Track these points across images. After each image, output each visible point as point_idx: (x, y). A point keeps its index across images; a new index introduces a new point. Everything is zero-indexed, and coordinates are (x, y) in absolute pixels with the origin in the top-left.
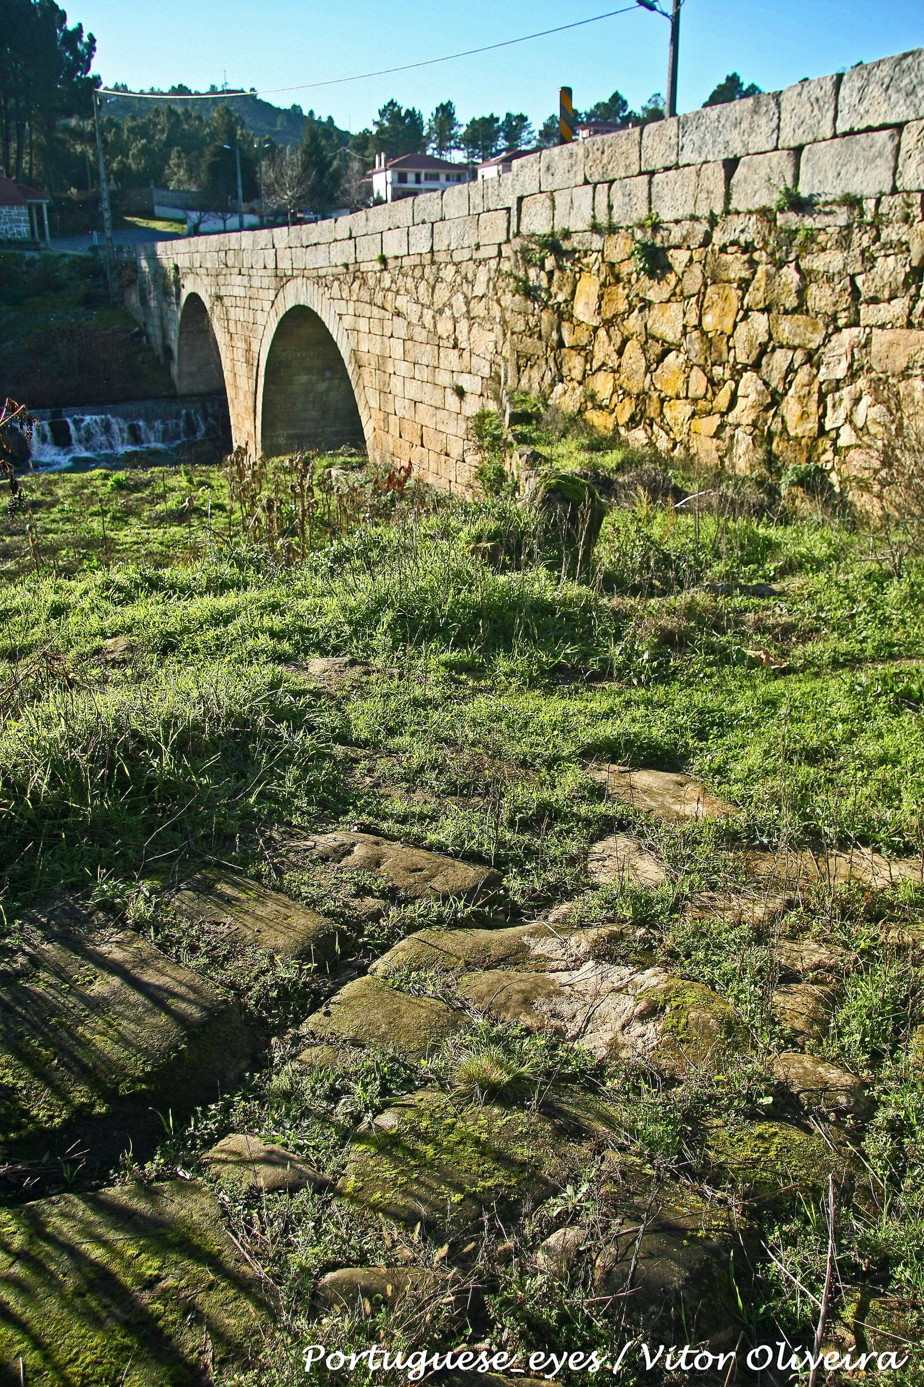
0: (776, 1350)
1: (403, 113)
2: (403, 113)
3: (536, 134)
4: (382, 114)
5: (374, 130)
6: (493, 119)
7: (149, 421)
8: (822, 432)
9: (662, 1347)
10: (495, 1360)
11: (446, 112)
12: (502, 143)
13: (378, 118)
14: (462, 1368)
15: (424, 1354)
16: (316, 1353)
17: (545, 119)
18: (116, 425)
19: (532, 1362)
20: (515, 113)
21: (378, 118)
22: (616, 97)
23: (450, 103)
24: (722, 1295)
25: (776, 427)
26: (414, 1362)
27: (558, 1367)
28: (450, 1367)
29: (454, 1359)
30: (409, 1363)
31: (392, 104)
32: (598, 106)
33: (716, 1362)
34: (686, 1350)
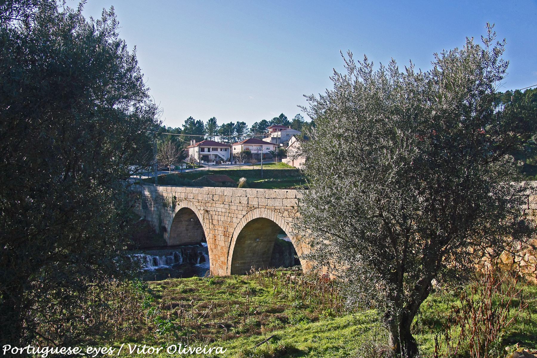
1: (196, 121)
2: (196, 121)
3: (249, 129)
4: (186, 122)
5: (183, 129)
6: (231, 124)
7: (161, 256)
8: (514, 262)
11: (213, 122)
12: (235, 134)
13: (184, 124)
15: (47, 348)
16: (8, 347)
17: (253, 124)
18: (149, 258)
20: (241, 121)
21: (184, 124)
22: (282, 115)
25: (499, 261)
26: (44, 351)
31: (191, 118)
32: (275, 119)
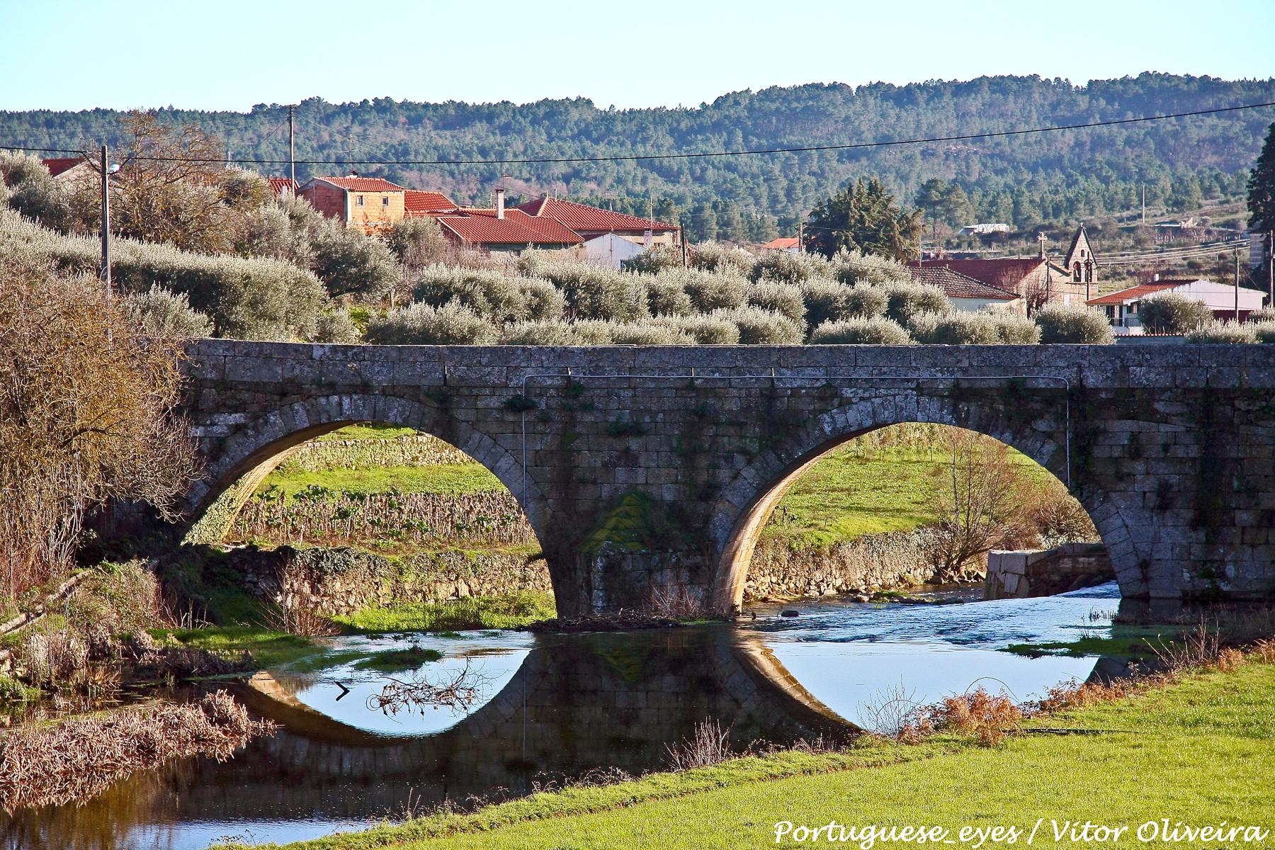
0: (1161, 825)
9: (1068, 823)
10: (931, 833)
14: (905, 840)
24: (194, 847)
27: (983, 839)
28: (895, 839)
29: (897, 834)
30: (861, 836)
33: (811, 835)
34: (1087, 826)
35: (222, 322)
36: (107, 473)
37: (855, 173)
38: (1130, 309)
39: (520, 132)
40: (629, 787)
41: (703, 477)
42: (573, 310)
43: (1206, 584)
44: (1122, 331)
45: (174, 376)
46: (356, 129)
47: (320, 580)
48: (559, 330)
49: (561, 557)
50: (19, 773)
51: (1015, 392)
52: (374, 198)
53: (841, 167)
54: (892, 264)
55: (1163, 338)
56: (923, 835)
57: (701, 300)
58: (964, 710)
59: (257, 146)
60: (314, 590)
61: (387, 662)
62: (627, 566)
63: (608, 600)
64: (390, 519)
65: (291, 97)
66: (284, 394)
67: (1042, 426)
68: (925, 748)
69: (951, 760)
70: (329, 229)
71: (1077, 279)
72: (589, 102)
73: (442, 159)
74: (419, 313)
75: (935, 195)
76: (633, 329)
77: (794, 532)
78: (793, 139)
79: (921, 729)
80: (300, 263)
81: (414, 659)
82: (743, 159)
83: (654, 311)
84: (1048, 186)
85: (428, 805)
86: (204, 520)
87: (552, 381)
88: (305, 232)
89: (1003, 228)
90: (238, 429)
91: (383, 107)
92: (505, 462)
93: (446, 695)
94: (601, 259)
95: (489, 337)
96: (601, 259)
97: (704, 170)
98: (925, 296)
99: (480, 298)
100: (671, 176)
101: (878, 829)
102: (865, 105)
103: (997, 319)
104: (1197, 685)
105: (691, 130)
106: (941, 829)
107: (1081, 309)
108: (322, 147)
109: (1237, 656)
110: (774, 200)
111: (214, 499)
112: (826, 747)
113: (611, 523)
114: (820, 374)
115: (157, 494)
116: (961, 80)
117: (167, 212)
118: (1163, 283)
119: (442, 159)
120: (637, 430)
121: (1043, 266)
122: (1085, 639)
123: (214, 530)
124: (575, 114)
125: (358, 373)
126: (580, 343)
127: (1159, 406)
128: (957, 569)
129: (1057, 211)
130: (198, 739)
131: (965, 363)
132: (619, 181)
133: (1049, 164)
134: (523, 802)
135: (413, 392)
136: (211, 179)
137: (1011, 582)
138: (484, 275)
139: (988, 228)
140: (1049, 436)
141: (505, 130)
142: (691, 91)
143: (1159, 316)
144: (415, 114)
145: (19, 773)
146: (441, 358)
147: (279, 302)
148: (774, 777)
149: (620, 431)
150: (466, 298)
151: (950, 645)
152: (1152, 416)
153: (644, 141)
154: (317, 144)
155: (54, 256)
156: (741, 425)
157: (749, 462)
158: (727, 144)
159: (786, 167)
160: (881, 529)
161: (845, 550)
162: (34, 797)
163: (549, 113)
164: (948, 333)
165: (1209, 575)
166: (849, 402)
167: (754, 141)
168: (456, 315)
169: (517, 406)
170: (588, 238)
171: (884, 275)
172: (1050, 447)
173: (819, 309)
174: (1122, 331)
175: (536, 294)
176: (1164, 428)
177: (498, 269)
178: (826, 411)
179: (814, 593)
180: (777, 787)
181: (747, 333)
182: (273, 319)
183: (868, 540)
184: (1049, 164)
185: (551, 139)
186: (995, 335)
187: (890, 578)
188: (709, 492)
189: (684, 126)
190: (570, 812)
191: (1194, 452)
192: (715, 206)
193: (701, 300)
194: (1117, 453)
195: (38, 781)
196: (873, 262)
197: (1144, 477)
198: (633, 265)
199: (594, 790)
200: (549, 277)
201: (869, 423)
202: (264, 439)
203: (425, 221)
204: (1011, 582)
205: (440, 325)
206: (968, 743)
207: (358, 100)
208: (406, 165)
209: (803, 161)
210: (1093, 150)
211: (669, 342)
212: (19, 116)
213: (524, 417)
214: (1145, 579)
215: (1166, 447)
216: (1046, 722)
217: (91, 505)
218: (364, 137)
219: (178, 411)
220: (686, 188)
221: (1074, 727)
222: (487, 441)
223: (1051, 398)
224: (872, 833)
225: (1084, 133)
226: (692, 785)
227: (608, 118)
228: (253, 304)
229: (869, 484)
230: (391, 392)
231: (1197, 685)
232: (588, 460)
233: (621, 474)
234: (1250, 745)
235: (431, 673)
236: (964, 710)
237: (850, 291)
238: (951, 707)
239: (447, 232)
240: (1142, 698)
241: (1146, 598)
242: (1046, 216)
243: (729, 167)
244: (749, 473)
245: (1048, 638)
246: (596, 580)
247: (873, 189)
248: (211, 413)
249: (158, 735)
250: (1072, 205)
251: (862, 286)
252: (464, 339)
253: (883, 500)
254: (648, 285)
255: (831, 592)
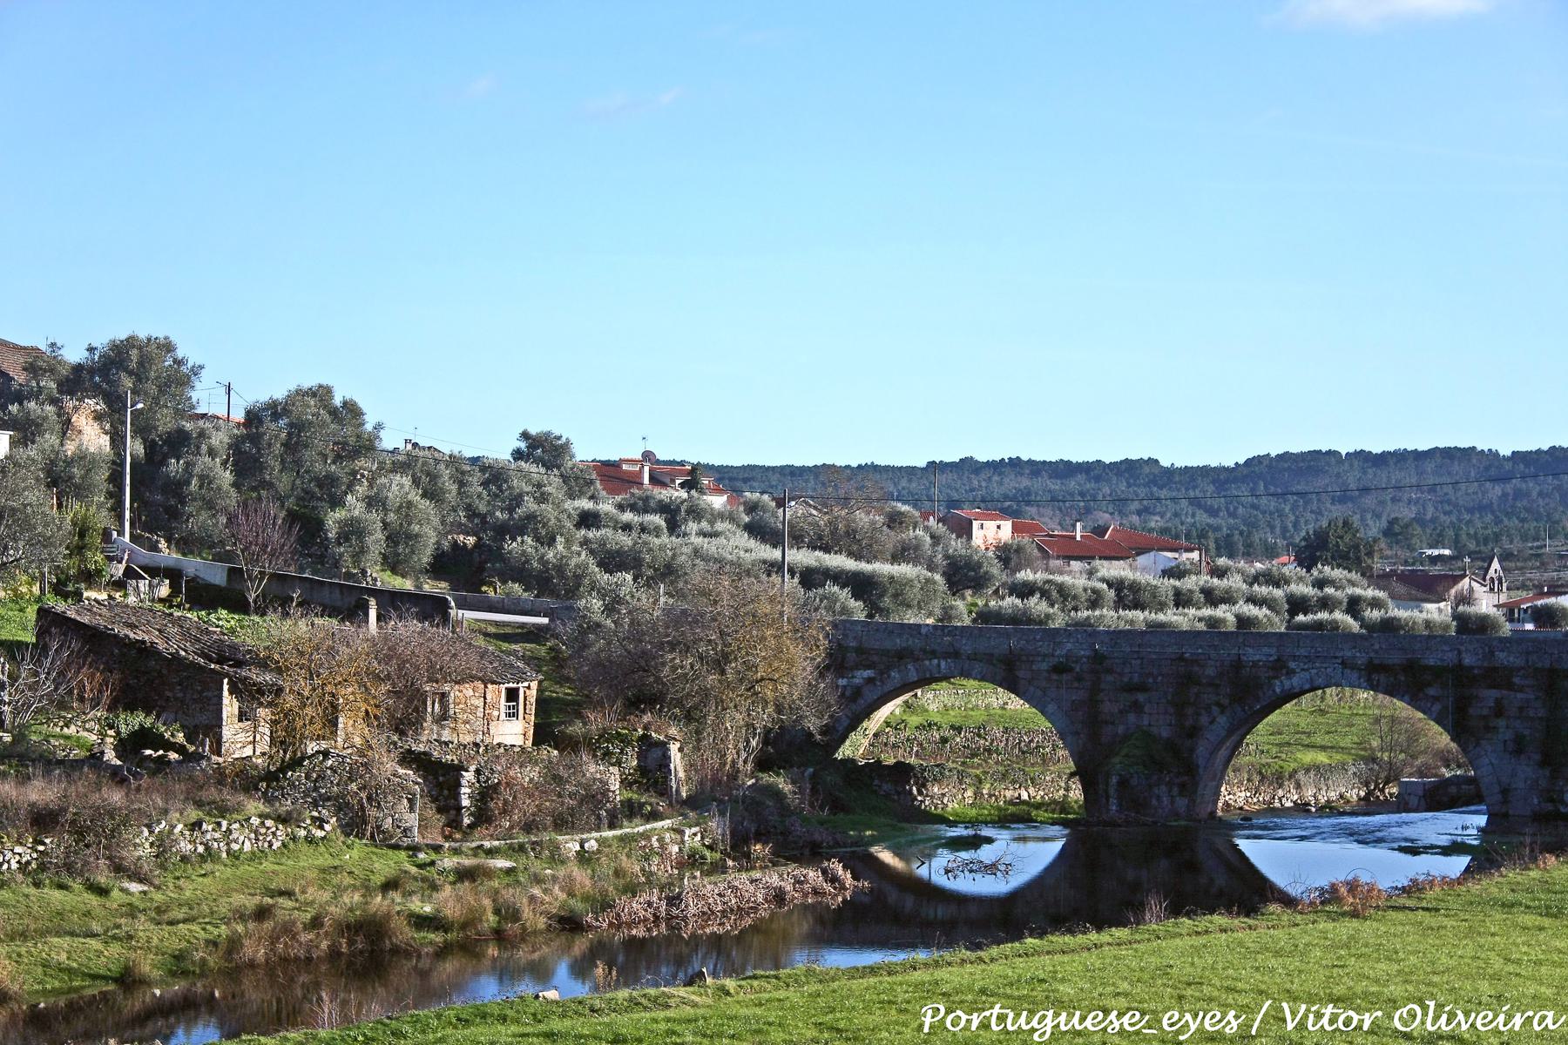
0: (1425, 1009)
10: (1126, 1020)
19: (1165, 1022)
23: (201, 367)
29: (1083, 1019)
30: (1034, 1023)
35: (873, 608)
36: (779, 709)
37: (1337, 512)
38: (1526, 611)
39: (1109, 481)
40: (1093, 936)
41: (1188, 723)
42: (1120, 603)
43: (1550, 807)
44: (1518, 627)
45: (824, 643)
46: (996, 478)
47: (924, 786)
48: (1109, 617)
49: (1086, 773)
50: (692, 910)
51: (1411, 667)
52: (990, 525)
53: (1333, 508)
54: (1354, 576)
55: (1548, 631)
56: (1115, 1022)
57: (1211, 597)
58: (1343, 890)
59: (928, 489)
60: (920, 793)
61: (957, 844)
62: (1134, 782)
63: (1120, 805)
64: (974, 747)
65: (953, 457)
66: (901, 658)
67: (1431, 692)
68: (1312, 917)
69: (1330, 925)
70: (956, 545)
71: (1492, 590)
72: (1157, 461)
73: (1053, 499)
74: (1011, 602)
75: (1397, 529)
76: (1161, 617)
77: (1264, 761)
78: (1300, 488)
79: (1312, 903)
80: (930, 569)
81: (975, 842)
82: (1264, 501)
83: (1177, 605)
84: (1481, 524)
85: (950, 944)
86: (847, 743)
87: (1084, 653)
88: (940, 548)
89: (1447, 552)
90: (870, 680)
91: (1016, 463)
92: (1051, 708)
93: (991, 869)
94: (1141, 570)
95: (1059, 622)
96: (1141, 570)
97: (1236, 508)
98: (1374, 598)
99: (1054, 594)
100: (1213, 512)
101: (1057, 1015)
102: (1351, 465)
103: (1424, 615)
104: (1519, 878)
105: (1227, 481)
106: (1138, 1015)
107: (1492, 611)
108: (972, 490)
109: (1551, 860)
110: (1284, 530)
111: (854, 728)
112: (1238, 914)
113: (1125, 751)
114: (1273, 651)
115: (813, 724)
116: (1420, 449)
117: (847, 533)
118: (1549, 594)
119: (1053, 499)
120: (1142, 688)
121: (1467, 580)
122: (1454, 843)
123: (855, 747)
124: (1146, 470)
125: (951, 644)
126: (1122, 626)
127: (1516, 680)
128: (1382, 791)
129: (1486, 541)
130: (816, 892)
131: (1377, 647)
132: (1176, 515)
133: (1482, 508)
134: (1017, 944)
135: (989, 658)
136: (880, 511)
137: (1414, 801)
138: (1059, 579)
139: (1436, 552)
140: (1436, 699)
141: (1098, 479)
142: (1229, 454)
143: (1545, 617)
144: (1036, 468)
145: (692, 910)
146: (1007, 635)
147: (914, 594)
148: (1198, 933)
149: (1131, 688)
150: (1045, 594)
151: (1355, 845)
152: (1510, 686)
153: (1194, 488)
154: (962, 486)
155: (765, 562)
156: (1218, 686)
157: (1222, 712)
158: (1252, 490)
159: (1294, 509)
160: (1327, 761)
161: (1301, 775)
162: (703, 927)
163: (1129, 468)
164: (1389, 625)
165: (1551, 800)
166: (1293, 672)
167: (1272, 489)
168: (1036, 605)
169: (1059, 669)
170: (1138, 554)
171: (1347, 583)
172: (1437, 707)
173: (1297, 605)
174: (1518, 627)
175: (1094, 591)
176: (1519, 695)
177: (1074, 576)
178: (1276, 677)
179: (1277, 805)
180: (1202, 940)
181: (1243, 621)
182: (909, 606)
183: (1317, 768)
184: (1482, 508)
185: (1129, 486)
186: (1422, 627)
187: (1333, 795)
188: (1194, 732)
189: (1219, 477)
190: (1048, 953)
191: (1542, 713)
192: (1241, 533)
193: (1211, 597)
194: (1485, 712)
195: (706, 916)
196: (1338, 573)
197: (1504, 730)
198: (1169, 573)
199: (1067, 938)
200: (1103, 580)
201: (1307, 686)
202: (888, 687)
203: (1025, 540)
204: (1414, 801)
205: (1025, 613)
206: (1344, 914)
207: (998, 459)
208: (1028, 503)
209: (1306, 503)
210: (1515, 499)
211: (1185, 627)
212: (774, 468)
213: (1065, 677)
214: (1505, 802)
215: (1521, 709)
216: (1403, 901)
217: (767, 731)
218: (1001, 483)
219: (827, 668)
220: (1223, 521)
221: (1424, 904)
222: (1039, 693)
223: (1438, 673)
224: (1048, 1020)
225: (1509, 488)
226: (1138, 937)
227: (1171, 472)
228: (896, 596)
229: (1324, 728)
230: (974, 657)
231: (1519, 878)
232: (1108, 707)
233: (1132, 718)
234: (1547, 922)
235: (986, 853)
236: (1343, 890)
237: (1320, 594)
238: (1334, 888)
239: (1040, 548)
240: (1493, 885)
241: (1506, 815)
242: (1478, 544)
243: (1255, 507)
244: (1222, 720)
245: (1427, 842)
246: (1112, 791)
247: (1346, 523)
248: (852, 669)
249: (789, 888)
250: (1497, 538)
251: (1329, 590)
252: (1041, 623)
253: (1325, 740)
254: (1174, 587)
255: (1289, 804)
